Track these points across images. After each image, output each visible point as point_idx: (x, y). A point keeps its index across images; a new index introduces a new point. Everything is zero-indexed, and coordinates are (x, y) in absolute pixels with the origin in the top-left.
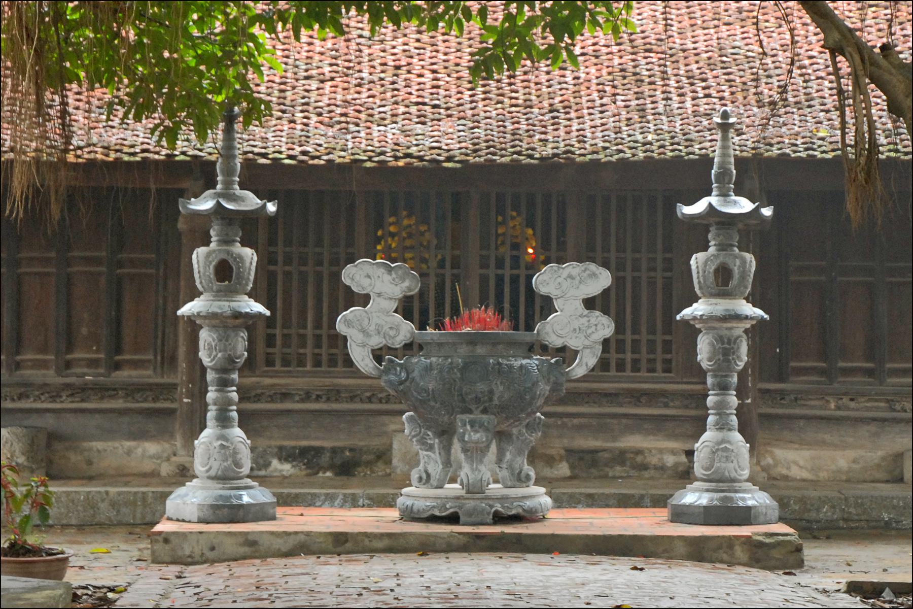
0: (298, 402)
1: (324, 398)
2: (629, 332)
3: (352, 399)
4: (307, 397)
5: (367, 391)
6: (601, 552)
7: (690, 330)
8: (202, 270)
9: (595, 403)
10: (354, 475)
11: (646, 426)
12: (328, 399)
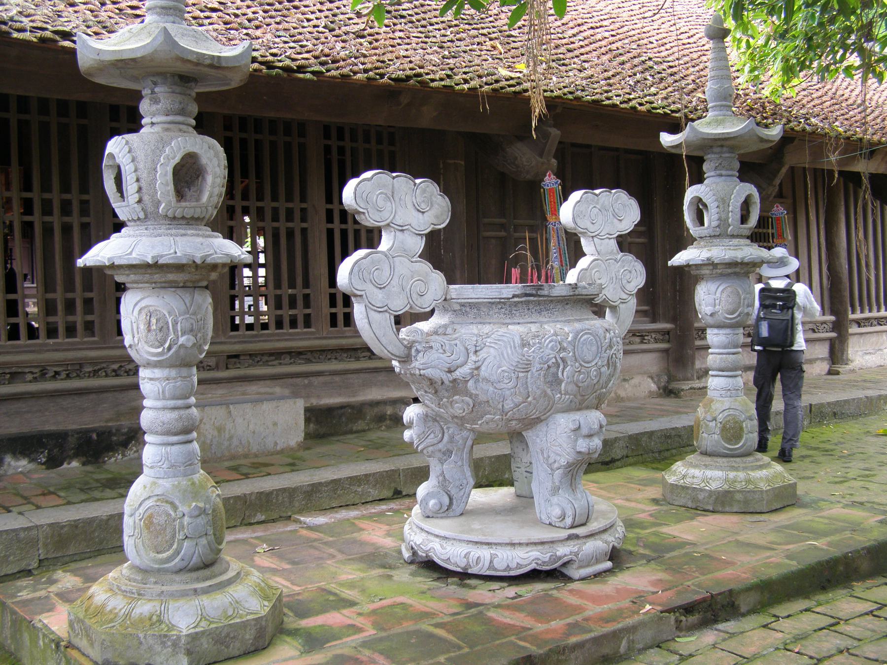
0: (30, 382)
1: (63, 375)
2: (60, 288)
3: (95, 373)
4: (43, 374)
5: (114, 362)
6: (824, 588)
7: (108, 286)
8: (144, 175)
9: (336, 359)
10: (809, 598)
11: (380, 378)
12: (68, 377)
